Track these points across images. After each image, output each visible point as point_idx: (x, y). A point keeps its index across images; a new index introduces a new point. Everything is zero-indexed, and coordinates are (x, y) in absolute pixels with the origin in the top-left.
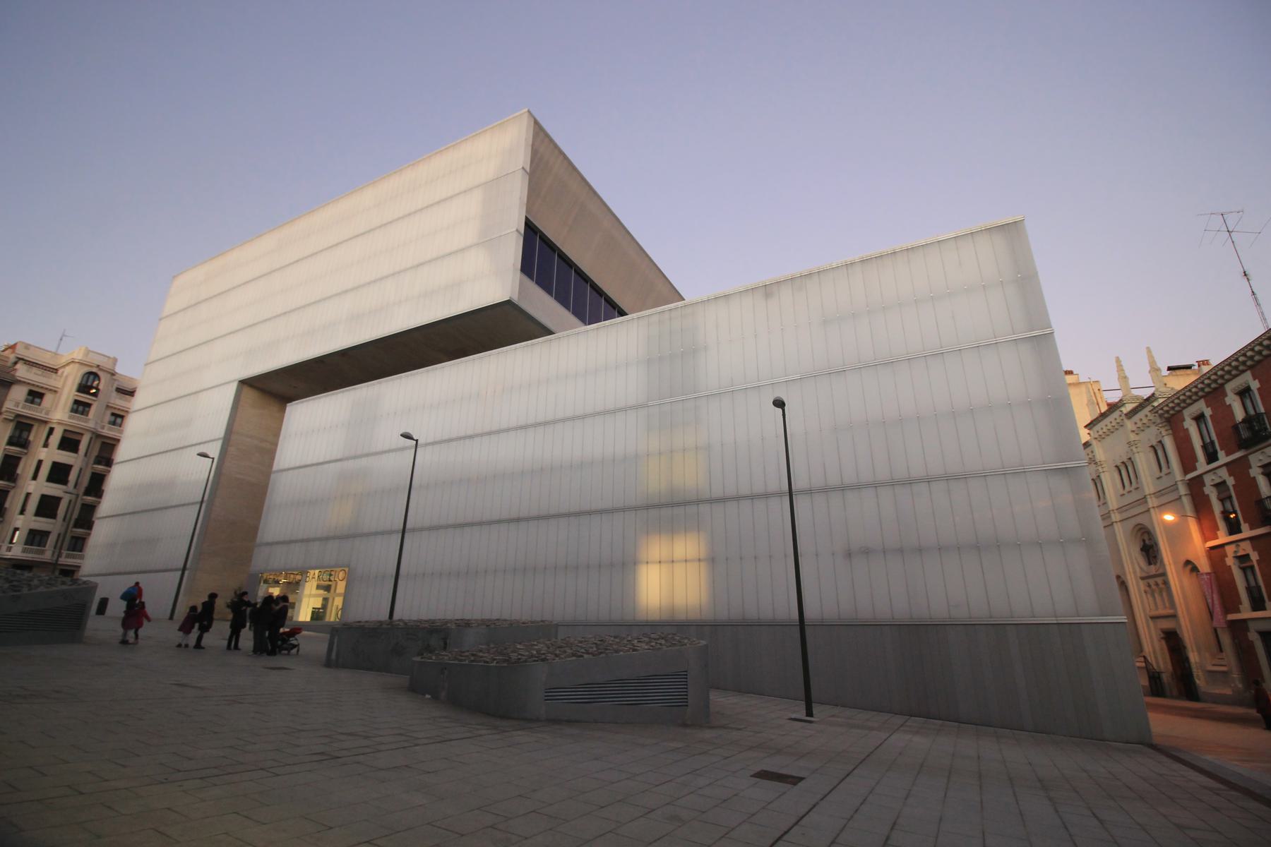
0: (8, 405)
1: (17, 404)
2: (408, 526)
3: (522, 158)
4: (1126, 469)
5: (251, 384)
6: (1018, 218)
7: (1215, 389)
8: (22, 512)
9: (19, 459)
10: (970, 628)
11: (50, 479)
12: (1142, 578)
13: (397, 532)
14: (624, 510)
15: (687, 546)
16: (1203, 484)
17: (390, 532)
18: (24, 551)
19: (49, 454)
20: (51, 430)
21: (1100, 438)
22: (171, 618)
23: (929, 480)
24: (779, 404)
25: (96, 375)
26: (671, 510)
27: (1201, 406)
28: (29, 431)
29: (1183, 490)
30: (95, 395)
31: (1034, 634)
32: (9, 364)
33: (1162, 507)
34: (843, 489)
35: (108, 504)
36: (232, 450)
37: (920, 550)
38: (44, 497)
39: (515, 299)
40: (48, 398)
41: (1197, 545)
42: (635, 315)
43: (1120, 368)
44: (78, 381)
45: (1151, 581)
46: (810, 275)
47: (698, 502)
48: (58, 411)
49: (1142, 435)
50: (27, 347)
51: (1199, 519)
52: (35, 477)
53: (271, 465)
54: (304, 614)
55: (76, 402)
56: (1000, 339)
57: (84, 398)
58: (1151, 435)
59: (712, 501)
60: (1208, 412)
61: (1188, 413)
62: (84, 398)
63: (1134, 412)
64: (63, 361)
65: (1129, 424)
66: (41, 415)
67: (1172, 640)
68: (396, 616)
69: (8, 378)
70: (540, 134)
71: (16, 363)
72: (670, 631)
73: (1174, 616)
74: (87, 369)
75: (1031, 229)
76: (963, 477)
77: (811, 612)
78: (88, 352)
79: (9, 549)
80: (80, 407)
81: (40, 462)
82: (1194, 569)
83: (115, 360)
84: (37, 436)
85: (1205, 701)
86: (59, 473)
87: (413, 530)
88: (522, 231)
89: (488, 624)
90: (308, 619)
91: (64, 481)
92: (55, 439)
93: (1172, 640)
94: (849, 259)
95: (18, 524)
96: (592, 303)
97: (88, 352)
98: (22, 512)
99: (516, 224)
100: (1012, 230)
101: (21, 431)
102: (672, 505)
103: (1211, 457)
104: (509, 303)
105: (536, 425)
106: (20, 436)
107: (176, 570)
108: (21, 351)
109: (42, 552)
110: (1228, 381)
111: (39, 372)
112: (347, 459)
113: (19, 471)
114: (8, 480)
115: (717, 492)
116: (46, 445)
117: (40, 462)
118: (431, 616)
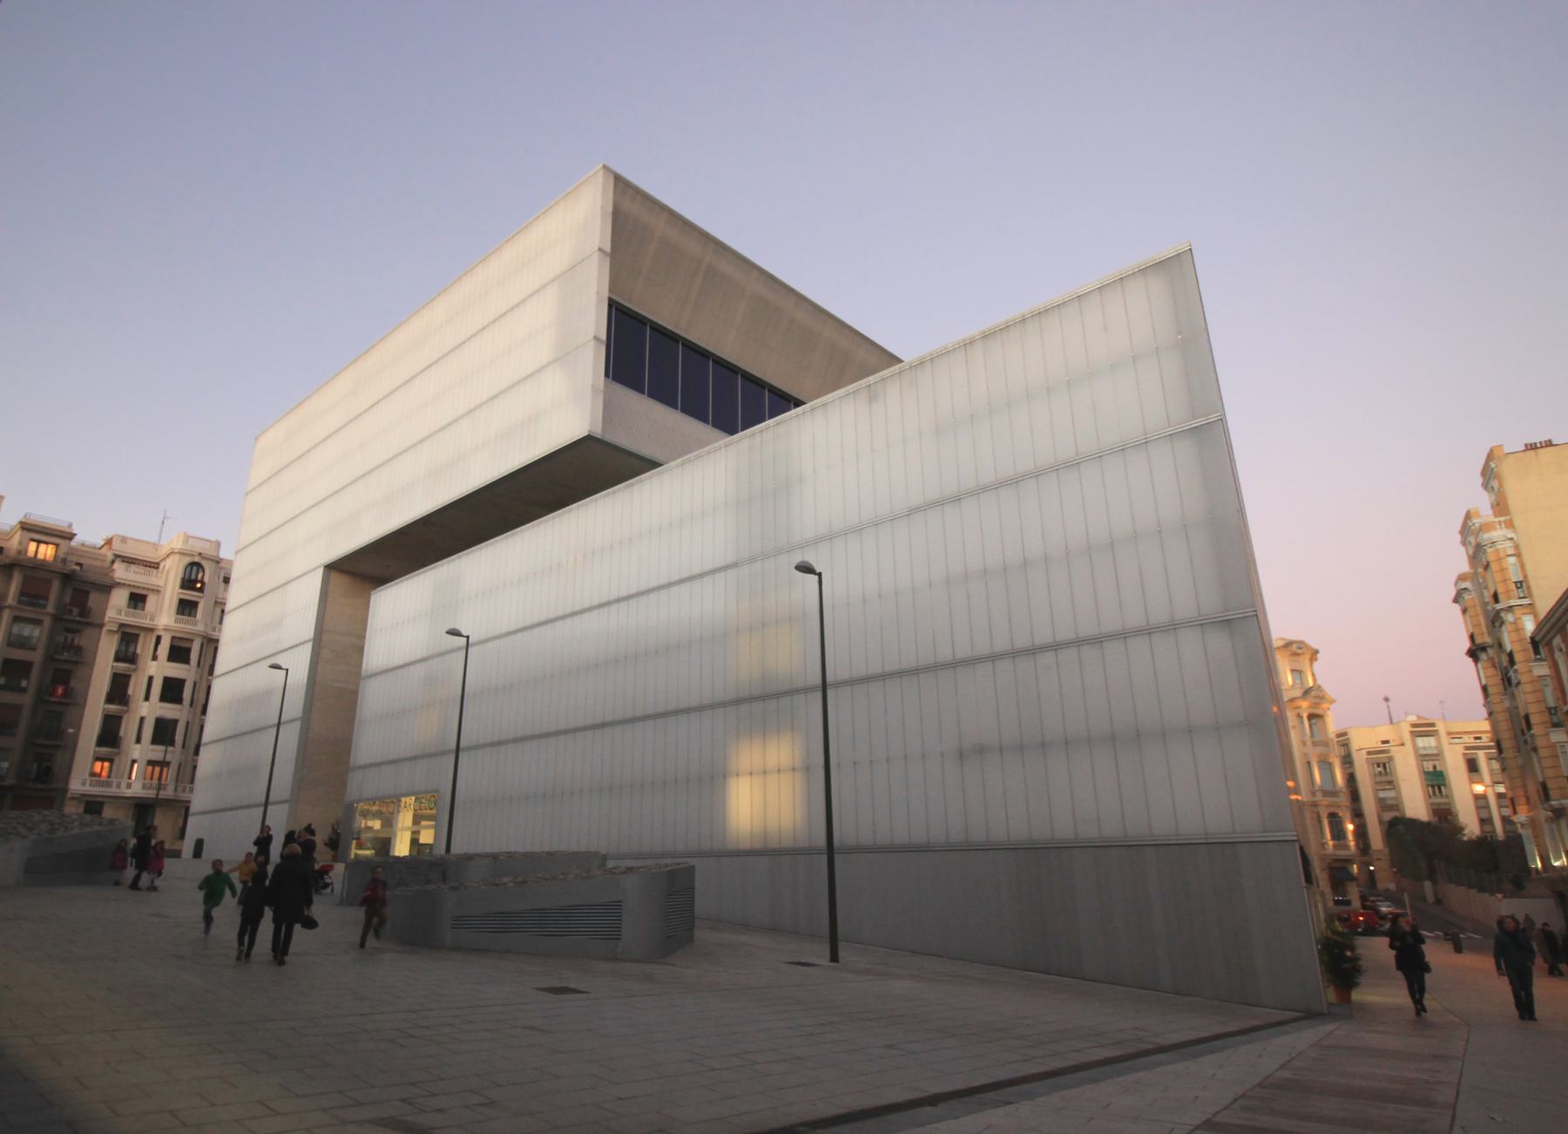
0: (111, 614)
1: (119, 612)
2: (462, 744)
3: (598, 234)
5: (336, 568)
8: (138, 741)
9: (128, 677)
10: (1101, 847)
14: (713, 706)
17: (443, 753)
18: (144, 787)
19: (158, 668)
20: (159, 639)
24: (806, 568)
25: (198, 565)
26: (758, 704)
30: (201, 590)
31: (1178, 852)
32: (107, 564)
35: (214, 725)
36: (325, 653)
39: (598, 432)
40: (151, 601)
42: (672, 464)
48: (163, 616)
50: (124, 540)
52: (147, 698)
54: (402, 848)
57: (190, 595)
62: (190, 595)
66: (146, 622)
68: (457, 848)
69: (107, 581)
70: (621, 185)
74: (188, 560)
77: (845, 832)
79: (129, 786)
80: (187, 608)
81: (151, 679)
83: (218, 544)
84: (144, 647)
86: (172, 690)
89: (495, 857)
97: (187, 538)
99: (593, 322)
100: (1176, 268)
101: (127, 646)
102: (764, 698)
104: (588, 440)
105: (619, 600)
107: (257, 806)
108: (118, 547)
111: (141, 569)
113: (130, 692)
116: (155, 658)
117: (151, 679)
118: (529, 848)
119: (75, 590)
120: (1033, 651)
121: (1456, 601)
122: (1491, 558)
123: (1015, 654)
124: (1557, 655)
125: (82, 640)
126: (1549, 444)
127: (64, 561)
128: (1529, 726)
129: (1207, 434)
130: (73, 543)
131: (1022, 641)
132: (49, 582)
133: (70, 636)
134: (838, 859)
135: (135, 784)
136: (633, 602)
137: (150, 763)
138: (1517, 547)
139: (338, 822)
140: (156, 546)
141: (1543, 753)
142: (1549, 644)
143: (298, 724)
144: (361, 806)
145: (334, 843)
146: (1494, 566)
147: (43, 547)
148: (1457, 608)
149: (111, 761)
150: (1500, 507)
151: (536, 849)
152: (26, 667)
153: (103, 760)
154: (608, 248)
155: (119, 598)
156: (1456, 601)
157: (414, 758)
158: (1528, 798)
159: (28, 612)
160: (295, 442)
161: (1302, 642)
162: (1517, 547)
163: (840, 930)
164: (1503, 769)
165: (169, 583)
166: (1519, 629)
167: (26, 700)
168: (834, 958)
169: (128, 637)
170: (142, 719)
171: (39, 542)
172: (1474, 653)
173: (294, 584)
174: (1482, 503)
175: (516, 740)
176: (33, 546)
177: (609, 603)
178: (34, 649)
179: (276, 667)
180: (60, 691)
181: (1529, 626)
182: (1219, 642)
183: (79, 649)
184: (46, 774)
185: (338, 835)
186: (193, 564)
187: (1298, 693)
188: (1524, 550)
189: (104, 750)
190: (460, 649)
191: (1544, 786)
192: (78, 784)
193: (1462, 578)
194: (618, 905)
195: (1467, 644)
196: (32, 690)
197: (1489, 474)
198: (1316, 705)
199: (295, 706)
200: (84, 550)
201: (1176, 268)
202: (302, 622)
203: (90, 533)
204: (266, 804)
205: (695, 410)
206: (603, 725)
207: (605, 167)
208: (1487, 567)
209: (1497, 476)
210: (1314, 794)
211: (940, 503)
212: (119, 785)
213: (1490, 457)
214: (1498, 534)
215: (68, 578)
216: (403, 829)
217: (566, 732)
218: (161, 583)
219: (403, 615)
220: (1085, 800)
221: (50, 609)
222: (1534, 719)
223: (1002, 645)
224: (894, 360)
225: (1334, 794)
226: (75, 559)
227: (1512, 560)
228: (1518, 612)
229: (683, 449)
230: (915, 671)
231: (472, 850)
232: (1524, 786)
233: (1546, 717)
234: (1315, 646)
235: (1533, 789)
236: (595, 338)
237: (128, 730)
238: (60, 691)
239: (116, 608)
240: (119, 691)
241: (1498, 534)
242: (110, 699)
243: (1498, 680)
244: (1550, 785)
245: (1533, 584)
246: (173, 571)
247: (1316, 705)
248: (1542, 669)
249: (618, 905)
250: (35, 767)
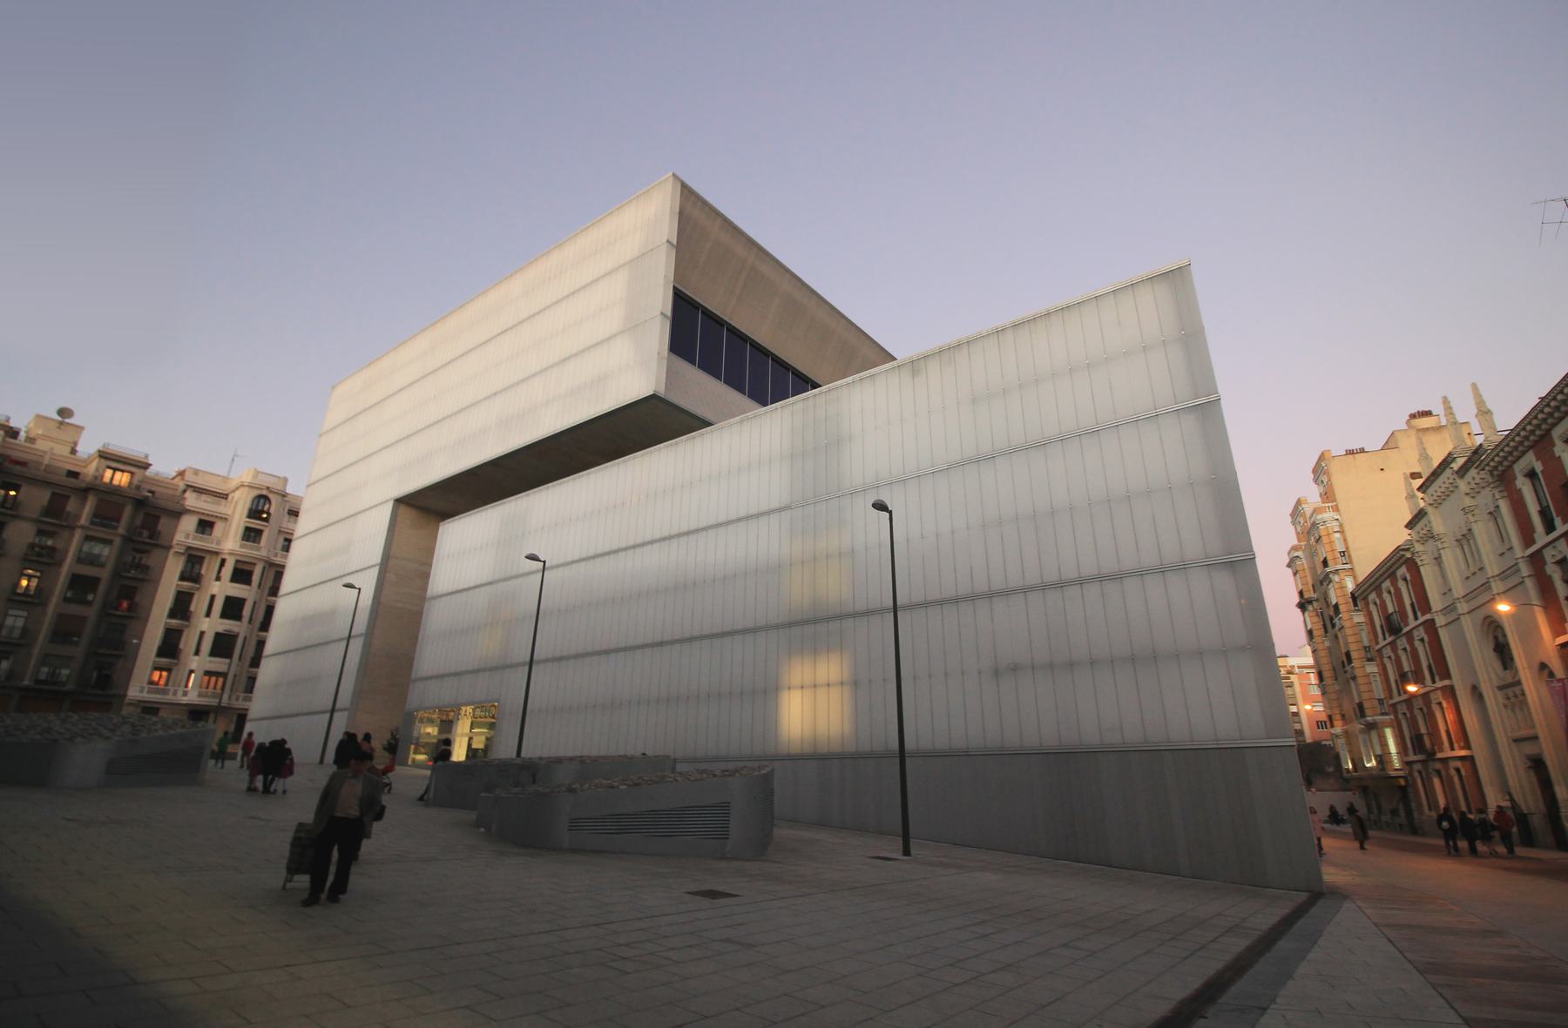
1: (187, 536)
3: (667, 229)
4: (1465, 539)
6: (1184, 263)
7: (1542, 437)
8: (197, 653)
9: (191, 595)
10: (1123, 755)
11: (224, 615)
12: (1500, 688)
13: (540, 662)
15: (831, 668)
16: (1544, 563)
18: (200, 695)
19: (221, 588)
20: (223, 561)
21: (1437, 504)
22: (321, 762)
23: (1081, 582)
24: (880, 506)
25: (266, 498)
26: (812, 627)
27: (1530, 460)
29: (1525, 570)
30: (266, 520)
32: (178, 493)
33: (1506, 594)
34: (991, 595)
35: (276, 639)
36: (390, 576)
37: (1071, 665)
38: (217, 634)
39: (662, 392)
41: (1549, 642)
43: (1480, 402)
44: (248, 505)
45: (1510, 692)
46: (959, 345)
47: (841, 617)
48: (229, 541)
49: (1479, 497)
50: (196, 472)
51: (1546, 608)
52: (208, 614)
53: (425, 588)
54: (459, 754)
55: (248, 529)
56: (1161, 410)
57: (255, 524)
58: (1487, 497)
59: (855, 615)
60: (1539, 467)
61: (1519, 468)
62: (255, 524)
63: (1463, 471)
64: (233, 484)
65: (1463, 485)
66: (212, 546)
67: (1537, 765)
68: (523, 754)
69: (177, 508)
70: (687, 193)
72: (820, 761)
73: (1535, 738)
74: (257, 492)
75: (1198, 276)
76: (1118, 577)
77: (910, 744)
78: (257, 473)
79: (185, 694)
80: (251, 535)
81: (213, 597)
82: (1551, 674)
83: (286, 480)
84: (209, 569)
85: (1424, 835)
86: (233, 608)
87: (540, 662)
88: (669, 313)
89: (582, 760)
91: (238, 617)
92: (227, 571)
93: (1537, 765)
94: (999, 324)
95: (194, 666)
96: (766, 376)
97: (257, 473)
98: (197, 653)
99: (661, 302)
100: (1176, 278)
102: (815, 621)
103: (1550, 527)
104: (653, 397)
108: (190, 478)
110: (1554, 425)
111: (210, 499)
113: (192, 608)
115: (860, 606)
116: (218, 578)
117: (213, 597)
119: (147, 514)
120: (1061, 585)
121: (1289, 566)
122: (1323, 533)
123: (1044, 587)
124: (1372, 607)
126: (1362, 451)
127: (138, 488)
128: (1350, 660)
129: (1206, 411)
130: (149, 472)
131: (1051, 576)
132: (123, 506)
134: (908, 761)
135: (191, 691)
136: (693, 537)
137: (208, 673)
138: (1341, 525)
139: (397, 729)
140: (226, 479)
141: (1361, 681)
142: (1365, 599)
145: (392, 748)
146: (1325, 540)
147: (118, 474)
148: (1289, 571)
149: (169, 670)
150: (1328, 495)
152: (92, 583)
153: (161, 669)
156: (1289, 566)
157: (477, 671)
158: (1343, 716)
159: (101, 533)
160: (360, 396)
162: (1341, 525)
164: (1324, 693)
165: (237, 513)
166: (1343, 587)
167: (91, 613)
168: (907, 852)
169: (194, 561)
170: (202, 633)
171: (115, 470)
172: (1302, 606)
173: (361, 516)
174: (1313, 495)
175: (577, 656)
176: (109, 473)
177: (670, 538)
178: (102, 566)
180: (125, 604)
181: (1350, 585)
182: (1224, 581)
183: (146, 568)
184: (105, 681)
185: (397, 740)
188: (1346, 528)
189: (164, 660)
190: (535, 572)
191: (1360, 706)
192: (136, 691)
193: (1294, 548)
194: (725, 807)
195: (1297, 599)
196: (96, 607)
197: (1320, 471)
199: (361, 626)
200: (155, 481)
201: (1176, 278)
202: (372, 550)
203: (164, 466)
204: (333, 711)
205: (735, 382)
208: (1318, 540)
209: (1327, 473)
211: (978, 460)
212: (175, 693)
213: (1322, 458)
214: (1328, 515)
215: (140, 503)
216: (462, 735)
217: (625, 649)
219: (469, 547)
220: (1107, 713)
221: (121, 530)
222: (1354, 655)
223: (1032, 578)
226: (148, 487)
228: (1342, 574)
230: (957, 600)
231: (561, 754)
232: (1340, 706)
235: (1348, 708)
237: (188, 643)
238: (125, 604)
239: (185, 532)
240: (181, 608)
241: (1328, 515)
242: (172, 615)
243: (1320, 625)
244: (1366, 705)
245: (1353, 554)
246: (239, 505)
248: (1359, 618)
249: (725, 807)
250: (95, 674)
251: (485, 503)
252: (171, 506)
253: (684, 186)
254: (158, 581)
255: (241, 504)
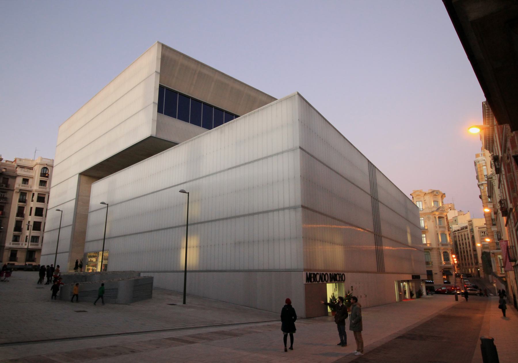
0: (16, 186)
5: (83, 174)
9: (24, 208)
19: (34, 204)
20: (33, 194)
25: (46, 168)
28: (26, 196)
30: (47, 177)
38: (35, 222)
40: (30, 181)
48: (35, 186)
50: (20, 160)
52: (30, 215)
57: (44, 179)
62: (44, 179)
64: (34, 163)
66: (29, 189)
69: (14, 175)
71: (17, 168)
74: (43, 166)
77: (188, 269)
78: (42, 159)
79: (26, 245)
80: (43, 183)
81: (31, 208)
83: (53, 160)
84: (29, 197)
87: (191, 224)
90: (38, 272)
92: (35, 198)
96: (209, 116)
97: (42, 159)
99: (153, 96)
104: (151, 137)
106: (23, 199)
108: (18, 162)
109: (37, 245)
111: (26, 170)
112: (190, 181)
113: (25, 213)
114: (21, 217)
116: (32, 201)
117: (31, 208)
119: (4, 178)
125: (7, 195)
133: (3, 194)
138: (486, 163)
143: (71, 227)
144: (89, 254)
151: (127, 270)
154: (159, 71)
155: (19, 180)
160: (73, 128)
161: (438, 191)
162: (486, 163)
163: (183, 296)
165: (36, 175)
169: (23, 193)
179: (59, 210)
186: (44, 168)
187: (435, 209)
198: (441, 213)
202: (72, 193)
204: (56, 253)
205: (195, 122)
206: (151, 231)
207: (158, 42)
210: (438, 245)
212: (22, 244)
218: (33, 175)
224: (273, 99)
225: (447, 245)
226: (4, 167)
227: (485, 167)
229: (187, 137)
233: (491, 222)
234: (443, 193)
236: (154, 103)
239: (18, 184)
240: (20, 212)
242: (18, 215)
247: (441, 213)
251: (111, 173)
252: (11, 174)
253: (163, 45)
254: (11, 203)
255: (37, 172)
